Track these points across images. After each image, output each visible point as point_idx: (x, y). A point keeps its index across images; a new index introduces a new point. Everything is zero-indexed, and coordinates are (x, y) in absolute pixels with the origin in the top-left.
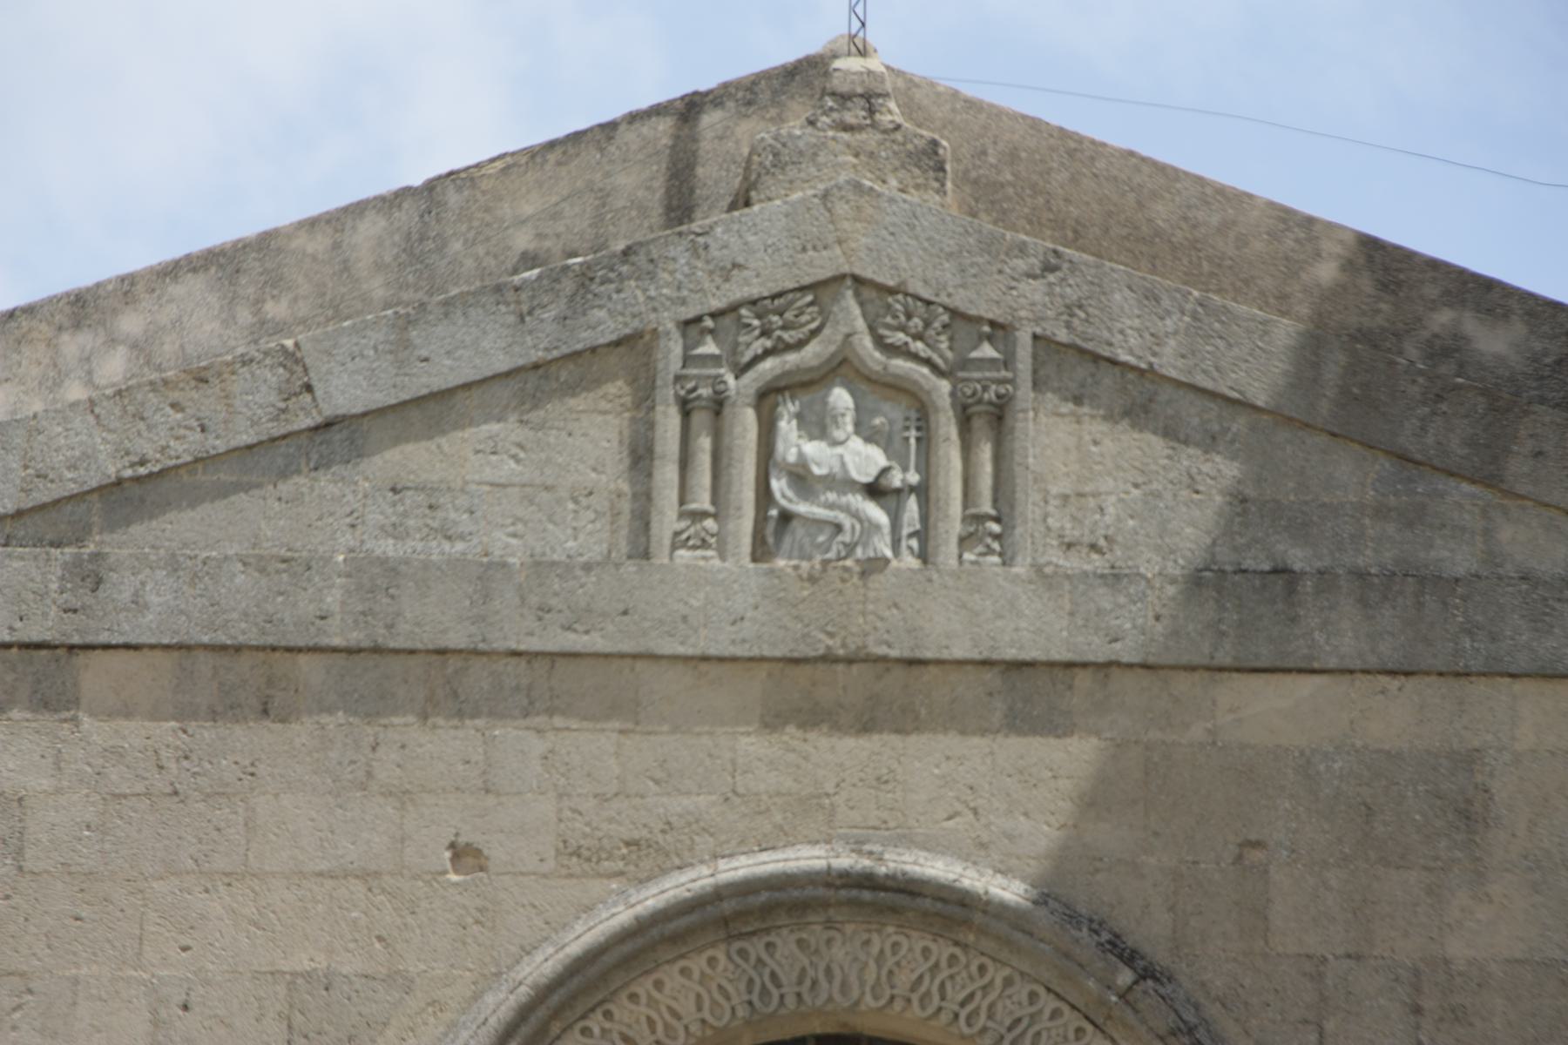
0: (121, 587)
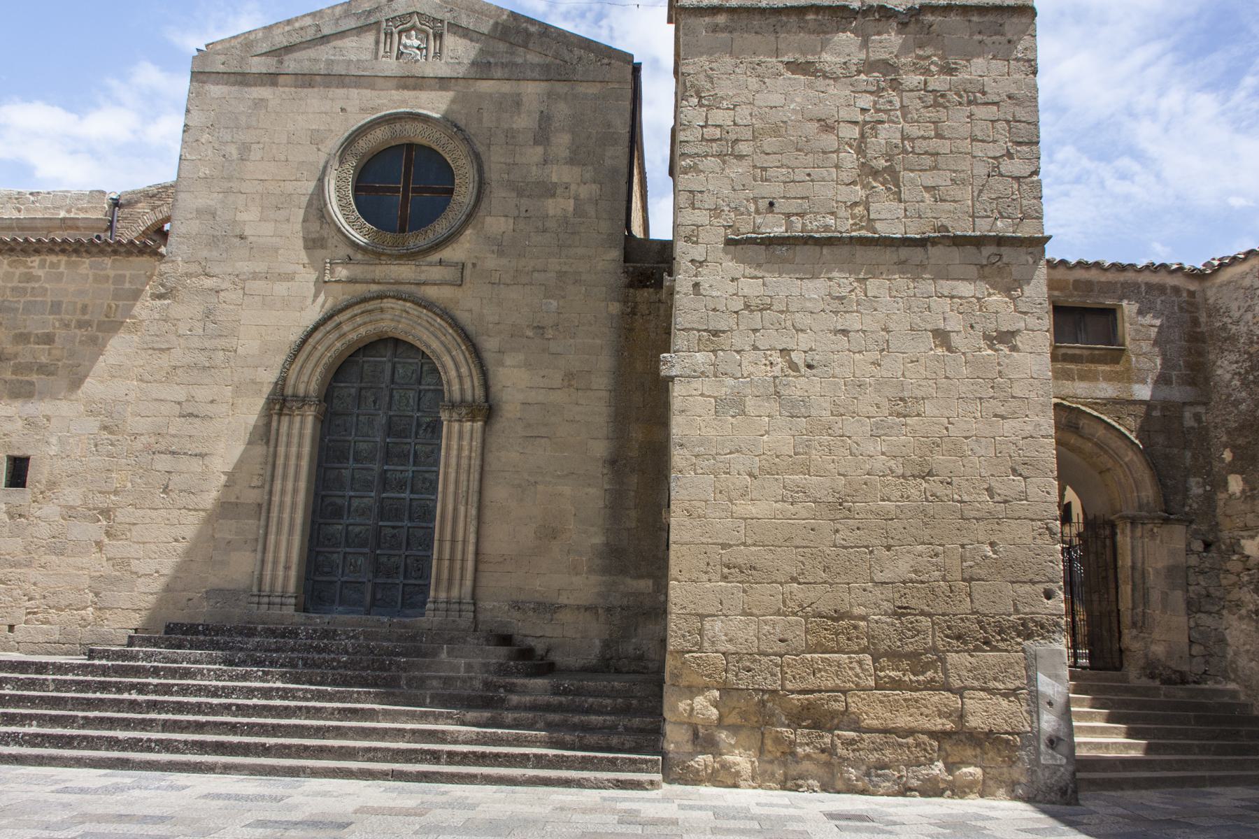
0: (286, 64)
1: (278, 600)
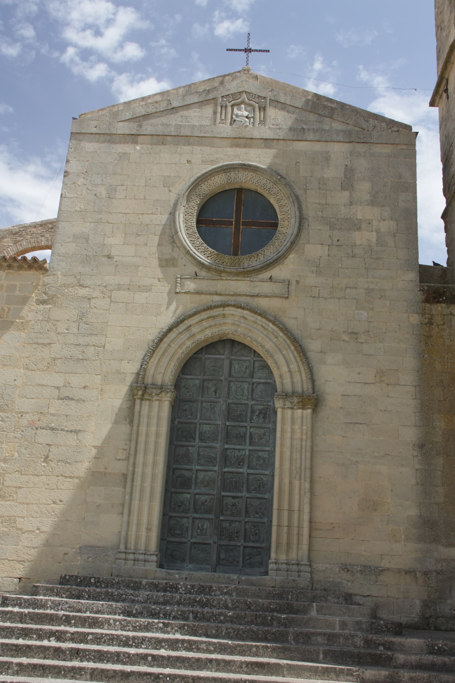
0: (144, 128)
1: (142, 557)
